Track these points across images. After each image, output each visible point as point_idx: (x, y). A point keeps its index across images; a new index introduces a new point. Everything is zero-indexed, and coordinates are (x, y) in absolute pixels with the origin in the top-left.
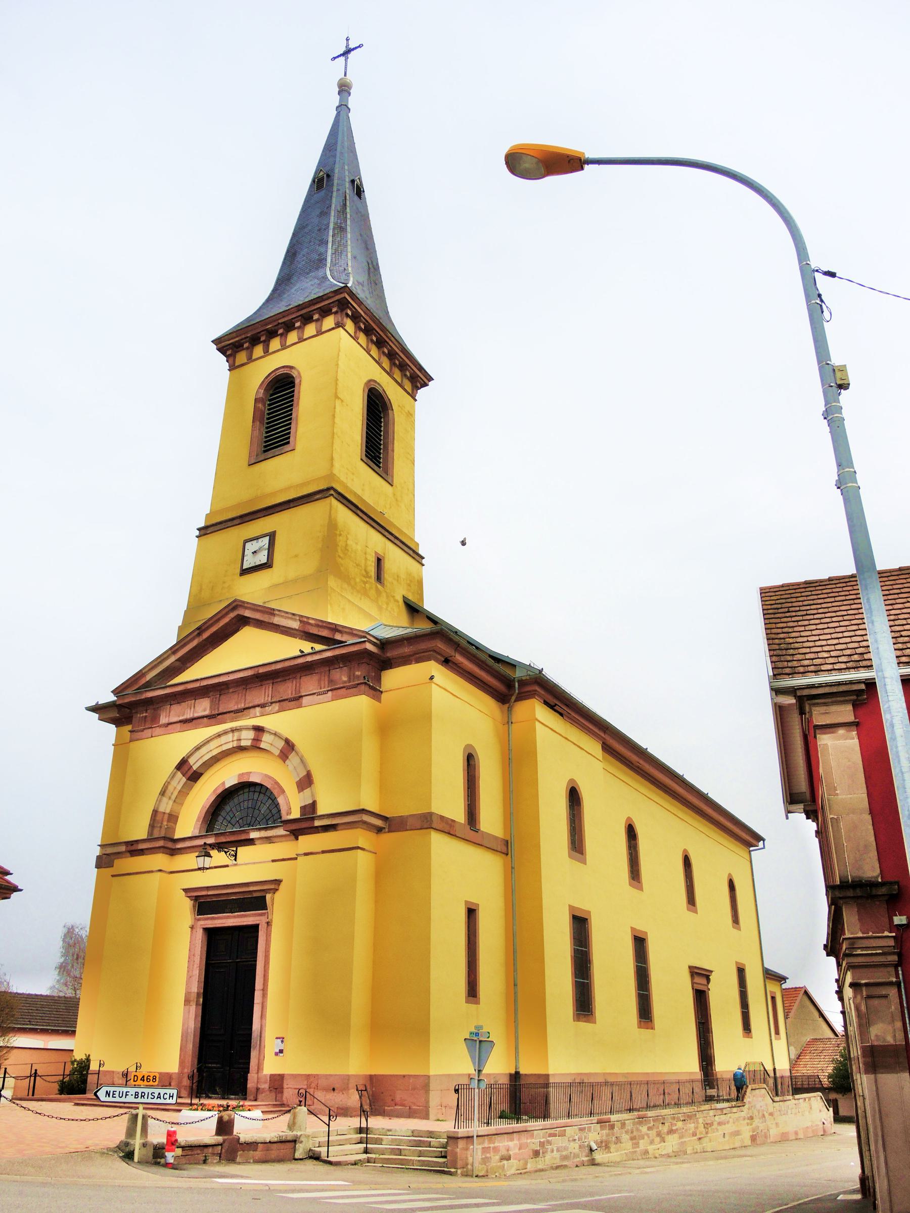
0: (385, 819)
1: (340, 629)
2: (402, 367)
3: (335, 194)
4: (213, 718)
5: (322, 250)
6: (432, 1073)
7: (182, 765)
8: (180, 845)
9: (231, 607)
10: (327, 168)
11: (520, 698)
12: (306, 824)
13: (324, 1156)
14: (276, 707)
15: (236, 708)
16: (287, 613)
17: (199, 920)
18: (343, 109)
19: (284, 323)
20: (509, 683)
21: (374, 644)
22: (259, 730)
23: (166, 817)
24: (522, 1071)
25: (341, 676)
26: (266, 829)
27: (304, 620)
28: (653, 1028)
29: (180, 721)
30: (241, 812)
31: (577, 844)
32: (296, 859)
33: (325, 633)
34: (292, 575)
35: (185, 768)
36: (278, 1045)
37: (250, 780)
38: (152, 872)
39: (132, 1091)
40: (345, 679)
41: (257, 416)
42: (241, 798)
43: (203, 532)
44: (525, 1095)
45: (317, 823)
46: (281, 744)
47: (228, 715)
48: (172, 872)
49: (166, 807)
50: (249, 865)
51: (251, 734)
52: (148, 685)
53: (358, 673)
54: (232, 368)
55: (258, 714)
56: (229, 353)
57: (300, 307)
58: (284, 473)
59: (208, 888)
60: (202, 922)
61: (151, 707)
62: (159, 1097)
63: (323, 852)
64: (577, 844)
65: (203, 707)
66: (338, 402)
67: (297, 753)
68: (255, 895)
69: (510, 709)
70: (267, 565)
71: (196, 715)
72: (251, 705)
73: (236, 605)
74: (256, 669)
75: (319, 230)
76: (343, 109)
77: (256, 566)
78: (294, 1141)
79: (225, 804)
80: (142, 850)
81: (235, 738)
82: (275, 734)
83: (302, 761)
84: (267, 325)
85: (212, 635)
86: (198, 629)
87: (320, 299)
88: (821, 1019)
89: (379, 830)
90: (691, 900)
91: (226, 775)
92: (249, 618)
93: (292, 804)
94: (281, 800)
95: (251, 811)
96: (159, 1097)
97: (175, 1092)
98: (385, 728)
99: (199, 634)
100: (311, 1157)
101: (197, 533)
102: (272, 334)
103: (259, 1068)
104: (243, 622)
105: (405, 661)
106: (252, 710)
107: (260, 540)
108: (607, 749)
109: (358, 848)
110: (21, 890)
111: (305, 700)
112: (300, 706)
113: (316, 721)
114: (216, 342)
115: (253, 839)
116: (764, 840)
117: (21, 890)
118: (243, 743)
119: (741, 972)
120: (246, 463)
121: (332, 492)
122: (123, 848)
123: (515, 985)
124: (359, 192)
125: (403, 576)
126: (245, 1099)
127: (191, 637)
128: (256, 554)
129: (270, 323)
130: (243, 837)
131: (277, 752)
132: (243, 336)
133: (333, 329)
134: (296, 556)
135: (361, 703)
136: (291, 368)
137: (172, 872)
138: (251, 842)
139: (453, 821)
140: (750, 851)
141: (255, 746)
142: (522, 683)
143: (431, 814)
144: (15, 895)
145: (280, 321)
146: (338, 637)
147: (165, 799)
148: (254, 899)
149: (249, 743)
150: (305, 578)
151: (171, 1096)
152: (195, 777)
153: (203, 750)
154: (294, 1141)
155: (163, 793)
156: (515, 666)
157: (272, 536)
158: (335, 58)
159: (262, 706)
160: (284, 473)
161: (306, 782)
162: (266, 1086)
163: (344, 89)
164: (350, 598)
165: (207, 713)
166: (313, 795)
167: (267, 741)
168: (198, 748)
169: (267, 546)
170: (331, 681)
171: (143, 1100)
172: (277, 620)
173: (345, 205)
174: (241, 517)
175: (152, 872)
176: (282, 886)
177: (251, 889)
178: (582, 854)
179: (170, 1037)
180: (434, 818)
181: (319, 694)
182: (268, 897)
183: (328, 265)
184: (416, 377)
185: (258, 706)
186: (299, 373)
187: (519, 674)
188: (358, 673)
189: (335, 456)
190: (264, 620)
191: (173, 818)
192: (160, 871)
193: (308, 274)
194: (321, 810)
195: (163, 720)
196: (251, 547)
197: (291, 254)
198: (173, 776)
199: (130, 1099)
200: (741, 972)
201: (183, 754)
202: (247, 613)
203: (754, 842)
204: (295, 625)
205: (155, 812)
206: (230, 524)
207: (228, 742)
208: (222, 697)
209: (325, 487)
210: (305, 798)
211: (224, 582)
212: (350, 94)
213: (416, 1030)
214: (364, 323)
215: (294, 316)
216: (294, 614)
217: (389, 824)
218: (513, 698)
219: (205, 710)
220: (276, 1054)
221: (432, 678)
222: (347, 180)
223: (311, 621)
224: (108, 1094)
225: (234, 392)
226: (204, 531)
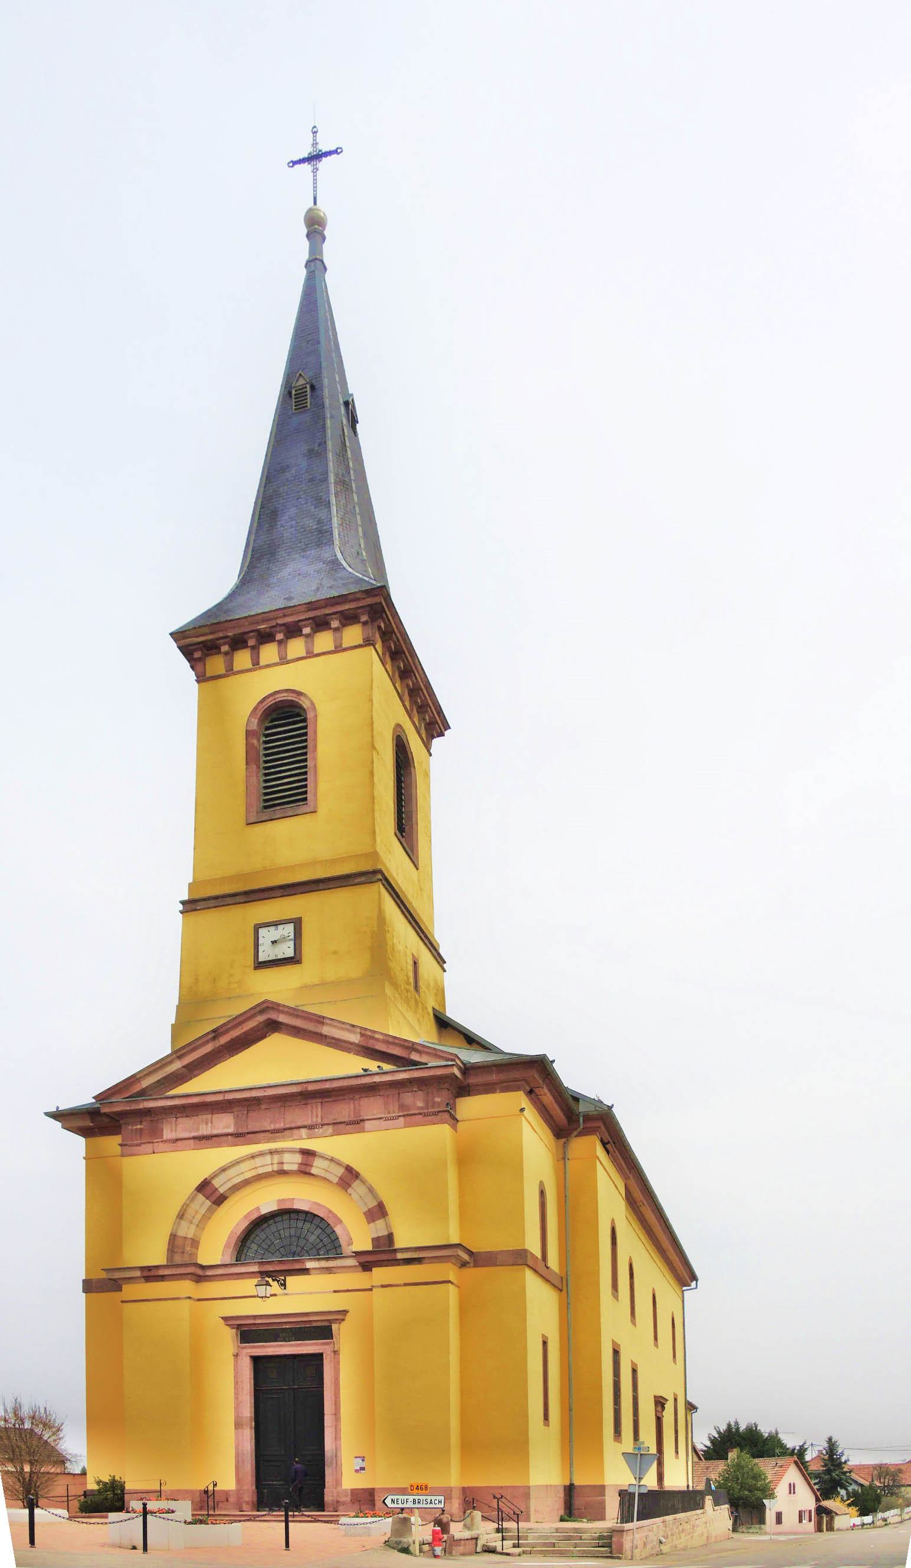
0: (470, 1253)
1: (419, 1048)
2: (422, 709)
3: (328, 422)
4: (240, 1137)
5: (322, 514)
6: (531, 1484)
7: (205, 1187)
8: (209, 1273)
9: (258, 1009)
10: (308, 375)
11: (580, 1134)
12: (382, 1254)
13: (499, 1549)
14: (330, 1129)
15: (272, 1127)
16: (344, 1023)
17: (244, 1348)
18: (315, 266)
19: (284, 625)
20: (571, 1115)
21: (460, 1068)
22: (308, 1153)
23: (189, 1242)
24: (576, 1483)
25: (416, 1100)
26: (327, 1259)
27: (364, 1032)
29: (194, 1138)
30: (283, 1240)
32: (371, 1290)
33: (396, 1051)
34: (331, 975)
35: (208, 1190)
36: (359, 1463)
37: (295, 1207)
38: (179, 1299)
39: (411, 1498)
40: (420, 1104)
41: (250, 758)
42: (280, 1226)
43: (188, 907)
44: (578, 1502)
46: (340, 1171)
47: (263, 1135)
48: (199, 1300)
50: (304, 1295)
51: (298, 1158)
52: (142, 1093)
53: (438, 1099)
54: (201, 678)
55: (304, 1136)
56: (197, 655)
57: (311, 606)
58: (294, 843)
59: (255, 1317)
60: (249, 1351)
61: (149, 1119)
63: (405, 1285)
65: (224, 1123)
66: (375, 754)
67: (364, 1182)
68: (314, 1324)
69: (565, 1146)
70: (294, 960)
71: (215, 1132)
72: (293, 1125)
73: (266, 1006)
74: (305, 1085)
75: (311, 480)
76: (315, 266)
77: (269, 961)
78: (476, 1539)
79: (258, 1232)
80: (163, 1276)
81: (275, 1161)
82: (332, 1160)
83: (371, 1190)
84: (258, 623)
85: (232, 1040)
86: (214, 1031)
87: (342, 599)
89: (464, 1264)
91: (266, 1199)
92: (281, 1023)
93: (358, 1236)
94: (338, 1230)
95: (294, 1239)
97: (442, 1498)
98: (466, 1159)
99: (214, 1038)
100: (485, 1551)
101: (181, 907)
102: (266, 637)
103: (338, 1482)
104: (274, 1026)
105: (488, 1088)
106: (295, 1131)
107: (280, 927)
111: (368, 1125)
112: (363, 1130)
113: (378, 1147)
114: (178, 636)
115: (308, 1270)
118: (286, 1167)
120: (243, 822)
121: (380, 877)
122: (138, 1274)
123: (570, 1410)
124: (353, 421)
125: (432, 984)
126: (324, 1511)
127: (204, 1040)
128: (275, 943)
129: (264, 621)
130: (298, 1266)
131: (335, 1180)
132: (221, 635)
133: (360, 646)
134: (335, 952)
135: (441, 1132)
136: (299, 694)
137: (199, 1300)
138: (305, 1271)
141: (304, 1171)
142: (587, 1118)
143: (526, 1251)
145: (280, 621)
146: (415, 1057)
147: (184, 1223)
148: (320, 1329)
149: (295, 1167)
150: (350, 981)
152: (220, 1200)
154: (476, 1539)
155: (181, 1216)
157: (297, 923)
159: (311, 1127)
160: (294, 843)
161: (378, 1212)
162: (348, 1499)
163: (315, 227)
164: (403, 1010)
165: (231, 1130)
166: (388, 1226)
167: (318, 1166)
168: (223, 1170)
169: (292, 937)
170: (402, 1107)
172: (326, 1030)
173: (344, 443)
174: (246, 893)
175: (179, 1299)
176: (348, 1317)
177: (312, 1318)
179: (226, 1456)
180: (529, 1256)
181: (387, 1119)
182: (334, 1327)
183: (337, 542)
184: (434, 723)
185: (305, 1127)
186: (313, 704)
187: (582, 1108)
188: (438, 1099)
189: (377, 829)
190: (309, 1029)
192: (189, 1298)
193: (304, 550)
194: (400, 1243)
195: (168, 1134)
196: (267, 935)
197: (267, 511)
198: (192, 1198)
199: (410, 1505)
201: (206, 1175)
202: (282, 1018)
204: (355, 1038)
205: (173, 1237)
206: (229, 900)
207: (267, 1164)
208: (251, 1114)
209: (370, 868)
210: (379, 1228)
211: (231, 975)
212: (324, 239)
213: (518, 1448)
214: (395, 643)
215: (302, 617)
216: (353, 1026)
217: (477, 1259)
218: (575, 1133)
219: (227, 1127)
220: (357, 1471)
221: (522, 1110)
222: (341, 401)
223: (377, 1036)
225: (211, 717)
226: (190, 906)
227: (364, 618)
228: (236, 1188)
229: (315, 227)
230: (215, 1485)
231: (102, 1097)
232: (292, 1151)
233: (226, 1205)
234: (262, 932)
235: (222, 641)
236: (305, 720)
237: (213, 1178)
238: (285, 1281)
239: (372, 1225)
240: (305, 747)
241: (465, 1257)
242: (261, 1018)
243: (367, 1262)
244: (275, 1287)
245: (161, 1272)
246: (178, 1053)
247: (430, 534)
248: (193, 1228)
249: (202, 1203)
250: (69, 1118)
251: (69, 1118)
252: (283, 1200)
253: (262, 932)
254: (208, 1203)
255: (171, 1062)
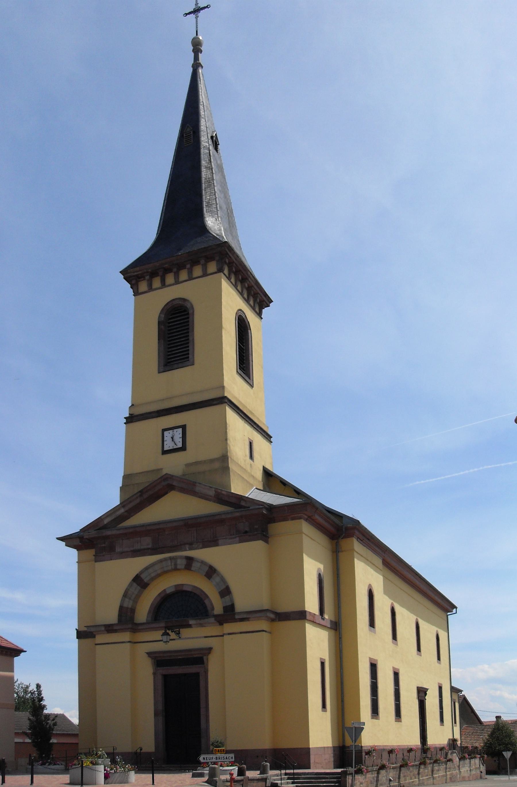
2: (255, 296)
8: (140, 628)
28: (401, 722)
31: (372, 624)
32: (223, 636)
45: (237, 617)
49: (128, 604)
52: (105, 527)
54: (136, 293)
62: (227, 758)
64: (372, 624)
71: (142, 547)
76: (196, 66)
80: (116, 630)
86: (140, 492)
88: (472, 714)
89: (273, 620)
90: (419, 649)
96: (227, 758)
101: (125, 421)
104: (170, 488)
108: (386, 563)
109: (263, 631)
110: (26, 651)
116: (456, 608)
117: (26, 651)
119: (440, 688)
133: (216, 273)
136: (184, 300)
137: (135, 643)
138: (189, 626)
139: (315, 614)
140: (447, 616)
144: (22, 654)
151: (232, 758)
153: (150, 570)
156: (342, 517)
157: (184, 428)
158: (187, 14)
160: (182, 383)
163: (197, 47)
167: (195, 566)
171: (219, 760)
178: (374, 628)
182: (205, 658)
185: (187, 544)
191: (133, 611)
195: (118, 549)
199: (214, 760)
200: (440, 688)
203: (450, 609)
224: (204, 759)
226: (130, 419)
227: (217, 258)
228: (153, 579)
229: (197, 47)
230: (141, 749)
231: (83, 530)
232: (181, 557)
233: (149, 588)
234: (166, 433)
235: (145, 274)
236: (188, 314)
237: (141, 574)
238: (179, 631)
239: (223, 599)
240: (188, 329)
241: (272, 616)
242: (164, 483)
243: (221, 620)
244: (173, 635)
245: (115, 628)
246: (123, 504)
247: (244, 211)
248: (131, 602)
249: (136, 589)
250: (69, 540)
251: (69, 540)
252: (178, 585)
253: (166, 433)
254: (139, 588)
255: (119, 509)
